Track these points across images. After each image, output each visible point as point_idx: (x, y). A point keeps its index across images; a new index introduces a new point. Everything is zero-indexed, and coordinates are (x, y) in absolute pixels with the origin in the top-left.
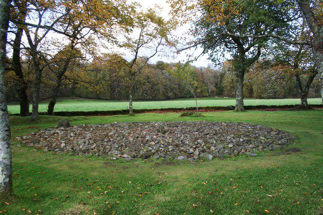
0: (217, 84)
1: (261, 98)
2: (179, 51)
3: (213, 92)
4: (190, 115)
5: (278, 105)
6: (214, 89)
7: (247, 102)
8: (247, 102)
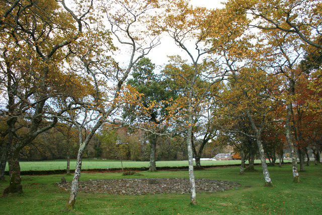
0: (96, 146)
1: (137, 160)
2: (303, 171)
3: (92, 153)
4: (132, 174)
5: (92, 167)
6: (94, 151)
7: (160, 164)
8: (160, 164)
